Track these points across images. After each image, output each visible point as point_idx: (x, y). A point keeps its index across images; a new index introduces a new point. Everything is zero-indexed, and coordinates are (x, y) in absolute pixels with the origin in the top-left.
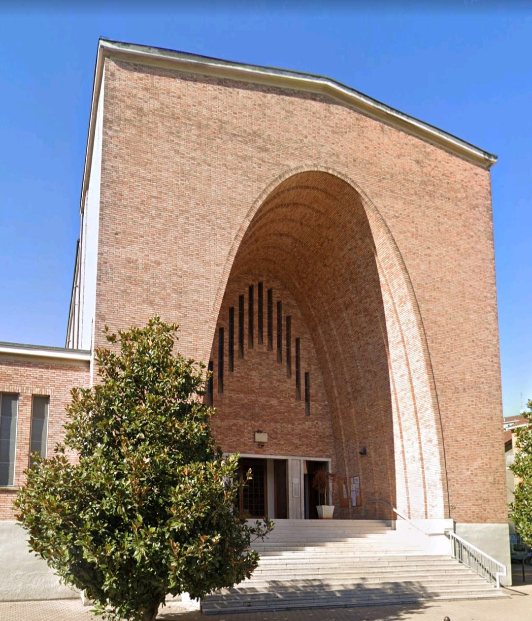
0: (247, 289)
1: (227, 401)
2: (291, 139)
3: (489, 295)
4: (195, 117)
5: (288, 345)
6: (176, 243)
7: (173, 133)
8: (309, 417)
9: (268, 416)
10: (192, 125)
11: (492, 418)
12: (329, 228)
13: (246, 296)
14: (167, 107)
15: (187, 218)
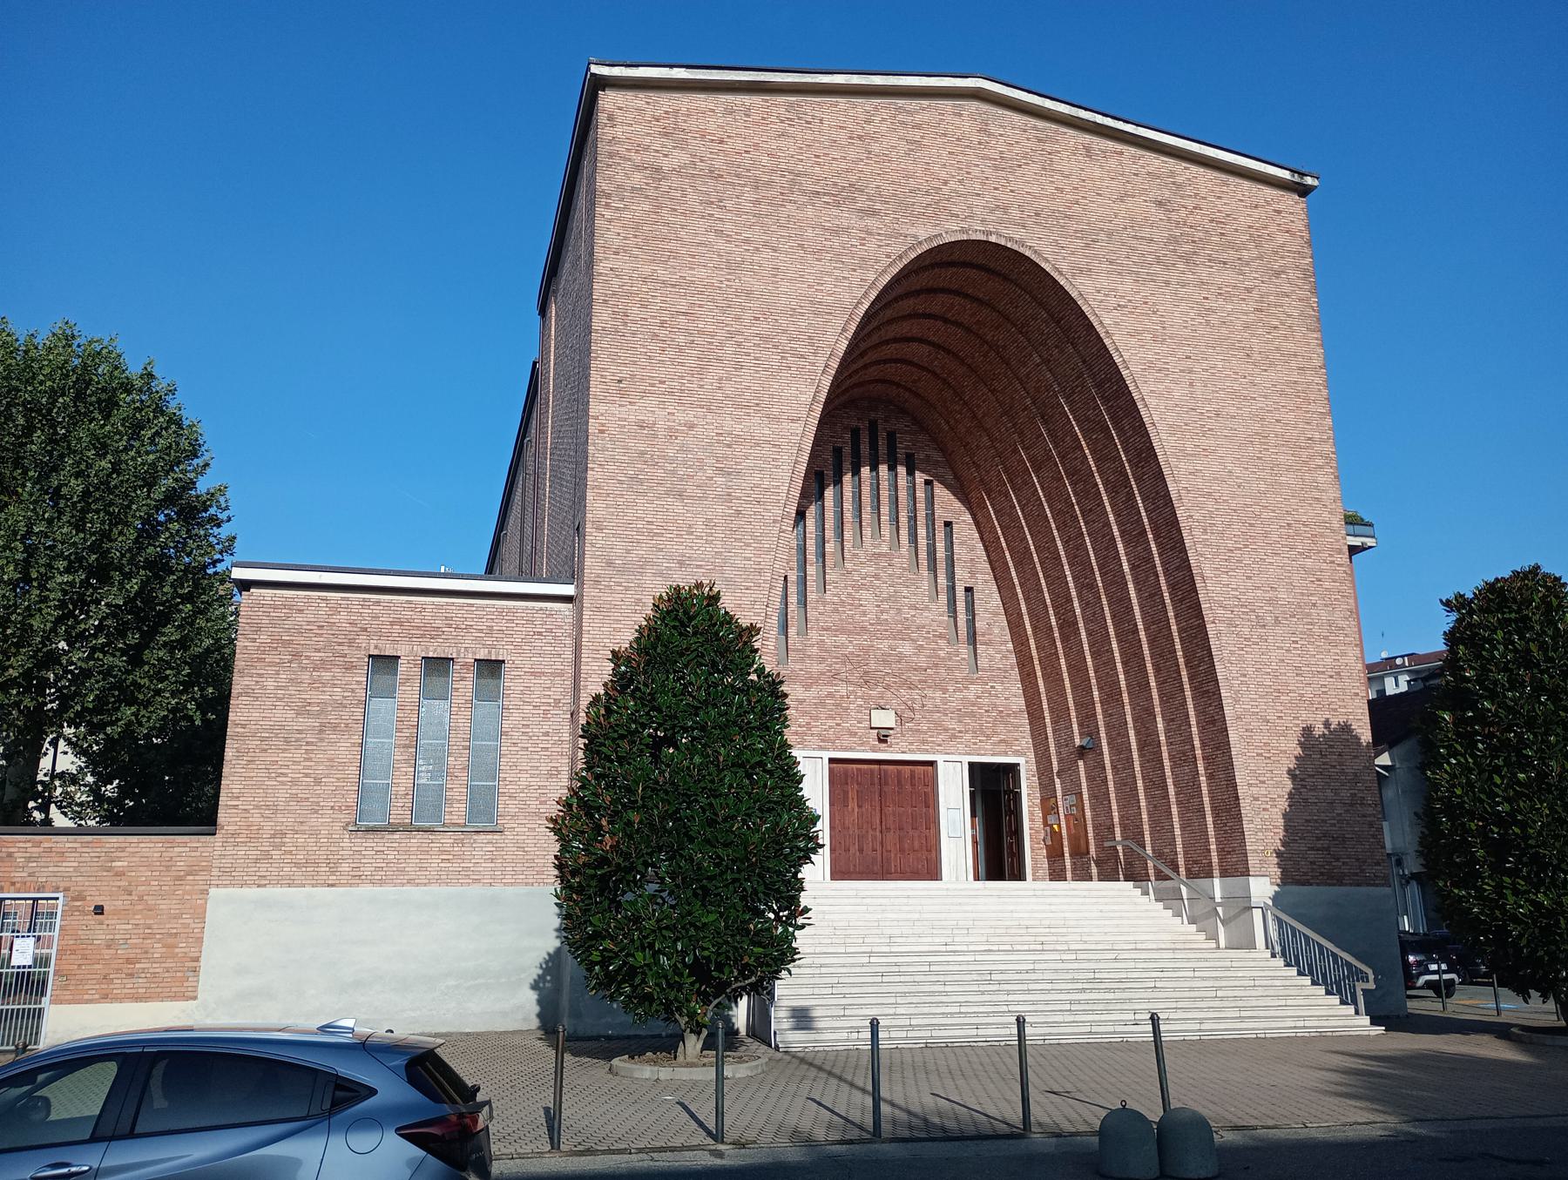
0: (848, 436)
1: (815, 650)
4: (749, 171)
5: (931, 536)
6: (720, 388)
7: (712, 203)
8: (976, 676)
11: (1338, 674)
12: (997, 328)
13: (847, 450)
14: (702, 161)
15: (739, 344)
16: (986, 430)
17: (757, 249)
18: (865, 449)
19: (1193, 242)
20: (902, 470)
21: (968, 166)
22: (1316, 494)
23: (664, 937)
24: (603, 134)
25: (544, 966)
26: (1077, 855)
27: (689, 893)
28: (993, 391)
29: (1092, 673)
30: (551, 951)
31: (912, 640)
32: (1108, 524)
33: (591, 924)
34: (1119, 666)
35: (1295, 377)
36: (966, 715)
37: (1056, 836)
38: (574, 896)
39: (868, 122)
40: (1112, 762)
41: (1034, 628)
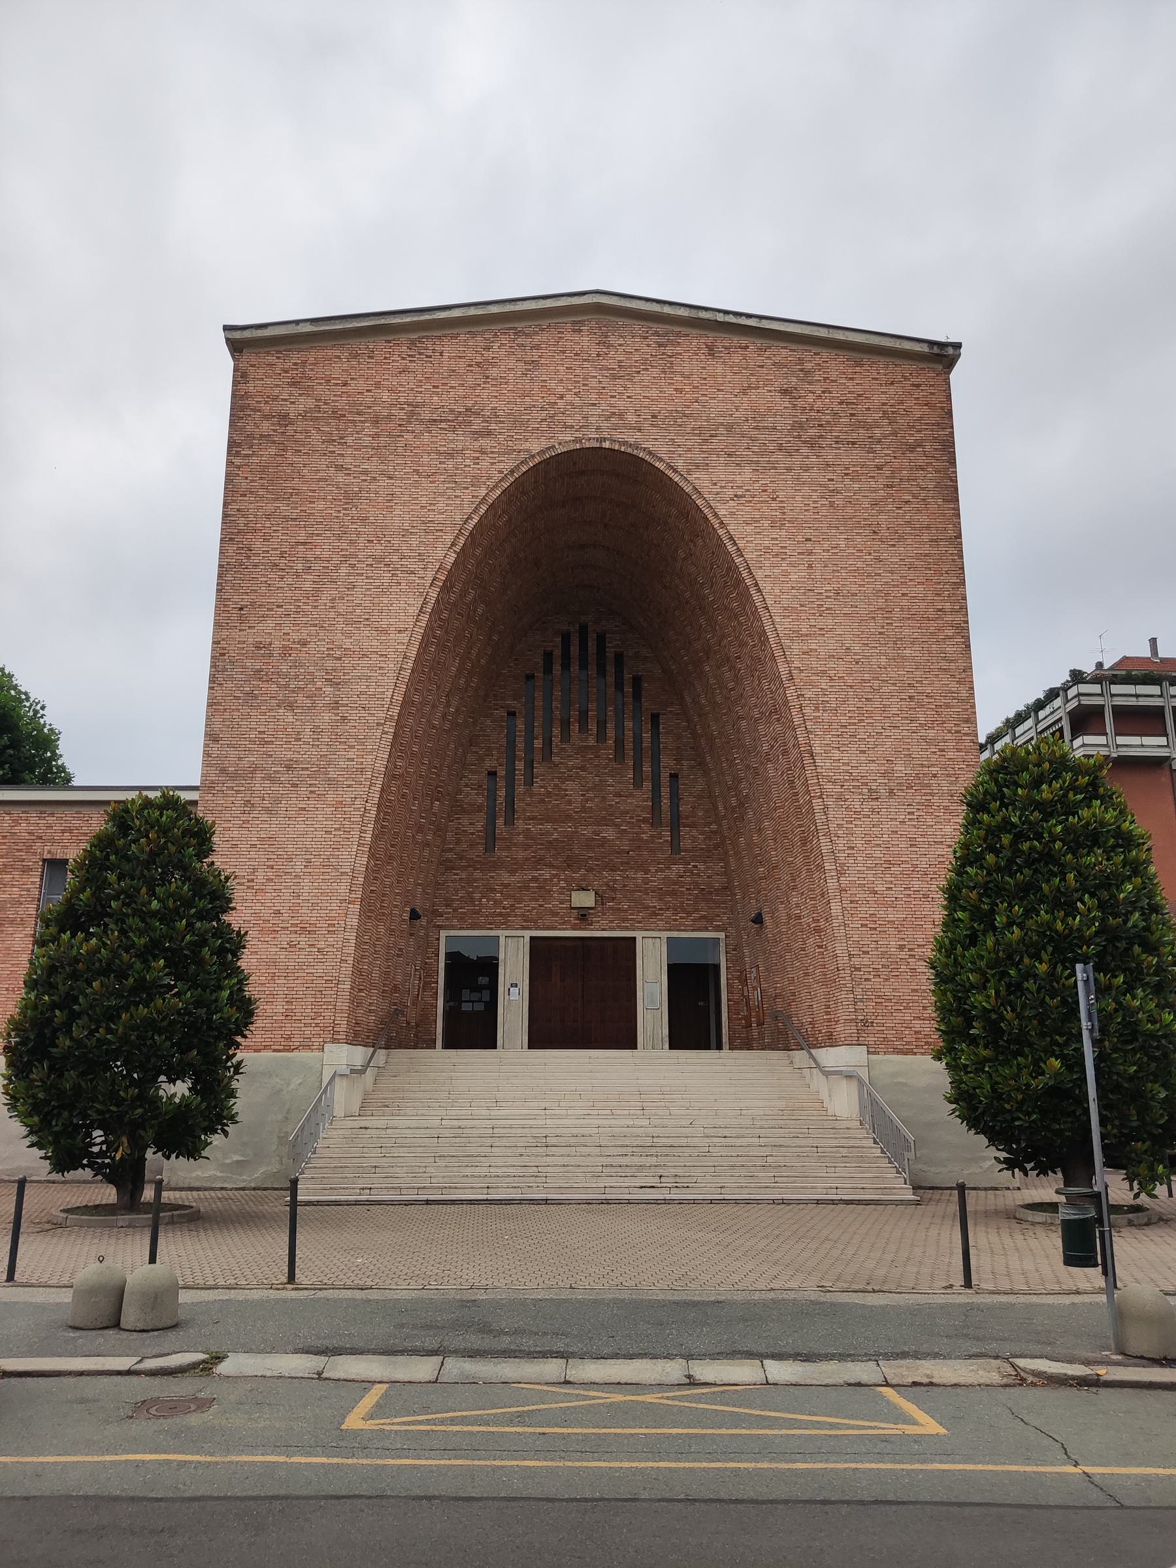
2: (534, 406)
3: (948, 606)
4: (370, 408)
6: (332, 607)
7: (334, 441)
9: (597, 860)
13: (558, 653)
14: (326, 404)
15: (353, 566)
17: (375, 478)
21: (585, 379)
22: (944, 665)
31: (616, 825)
35: (926, 549)
39: (487, 349)
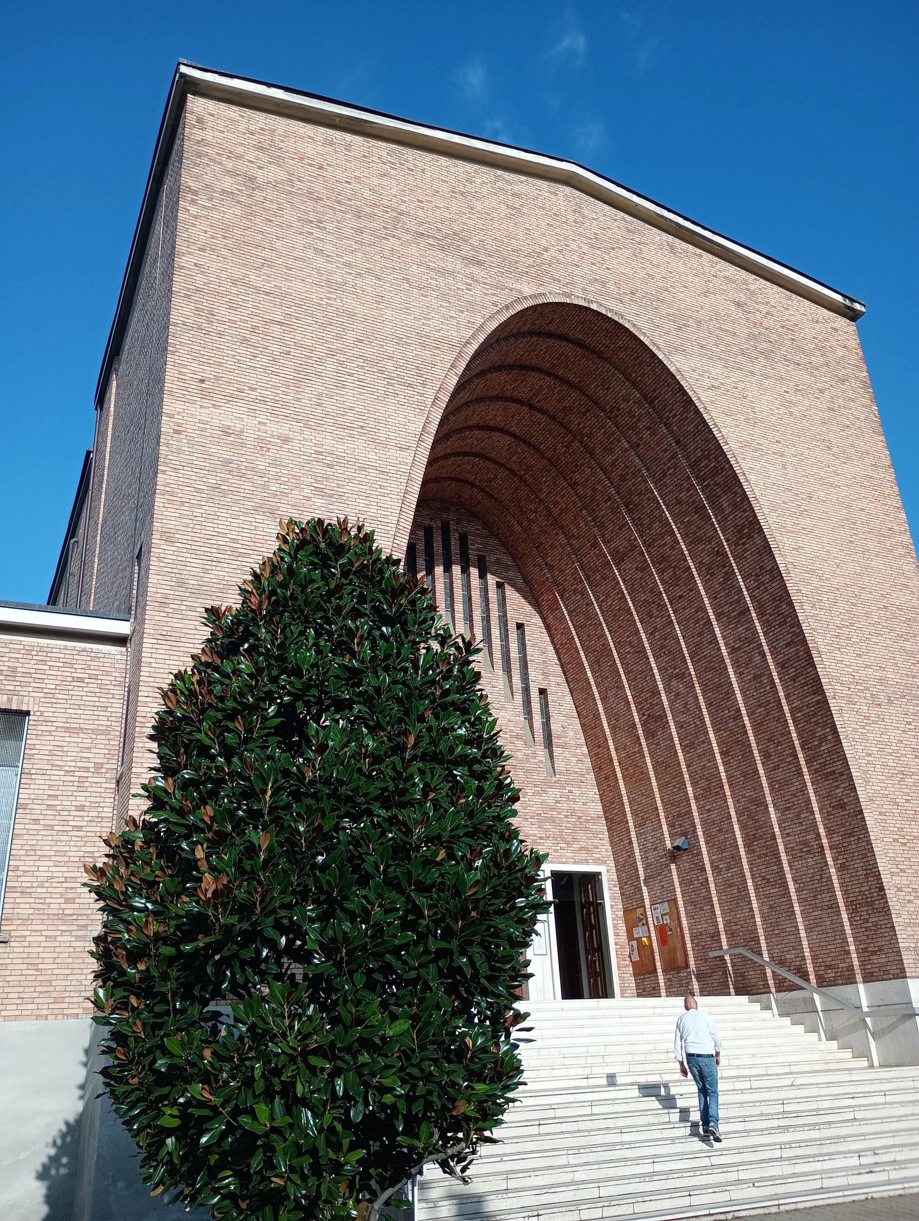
5: (505, 637)
7: (311, 222)
8: (554, 779)
10: (345, 212)
12: (584, 414)
14: (300, 181)
15: (341, 363)
16: (561, 528)
18: (438, 547)
19: (769, 341)
20: (474, 572)
22: (904, 581)
23: (312, 1069)
24: (191, 134)
25: (59, 1142)
26: (672, 970)
27: (360, 979)
28: (573, 485)
29: (684, 769)
30: (71, 1119)
32: (703, 609)
33: (165, 1052)
34: (718, 756)
36: (547, 820)
37: (644, 950)
38: (134, 1001)
40: (712, 863)
41: (613, 728)
